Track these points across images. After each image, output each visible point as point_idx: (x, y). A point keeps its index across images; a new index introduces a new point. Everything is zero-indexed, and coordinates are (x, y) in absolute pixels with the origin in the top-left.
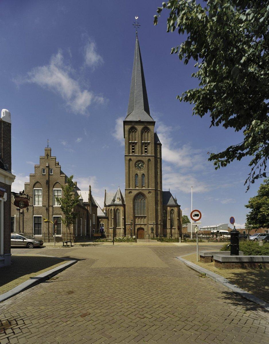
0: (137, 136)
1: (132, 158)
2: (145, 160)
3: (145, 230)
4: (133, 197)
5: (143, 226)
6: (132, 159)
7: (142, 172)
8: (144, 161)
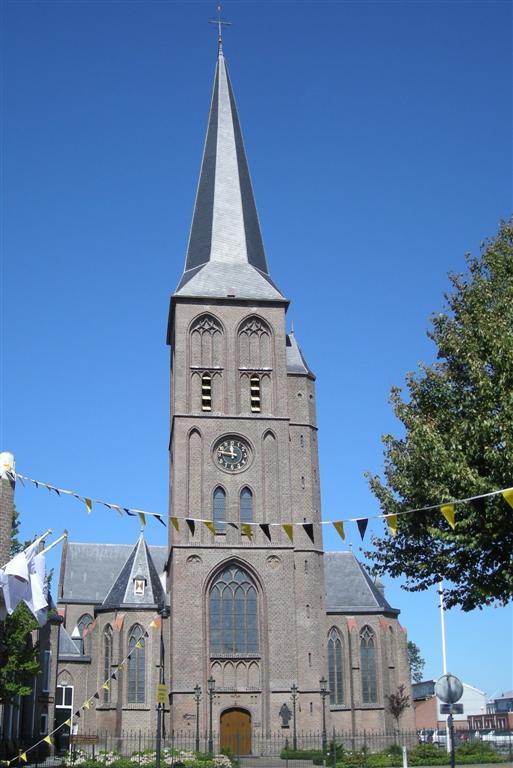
0: (220, 347)
1: (200, 424)
2: (252, 431)
3: (257, 717)
4: (204, 578)
5: (244, 702)
6: (203, 431)
7: (243, 479)
8: (250, 439)
